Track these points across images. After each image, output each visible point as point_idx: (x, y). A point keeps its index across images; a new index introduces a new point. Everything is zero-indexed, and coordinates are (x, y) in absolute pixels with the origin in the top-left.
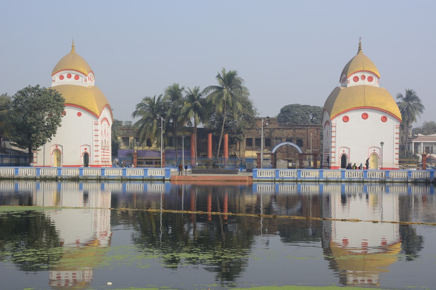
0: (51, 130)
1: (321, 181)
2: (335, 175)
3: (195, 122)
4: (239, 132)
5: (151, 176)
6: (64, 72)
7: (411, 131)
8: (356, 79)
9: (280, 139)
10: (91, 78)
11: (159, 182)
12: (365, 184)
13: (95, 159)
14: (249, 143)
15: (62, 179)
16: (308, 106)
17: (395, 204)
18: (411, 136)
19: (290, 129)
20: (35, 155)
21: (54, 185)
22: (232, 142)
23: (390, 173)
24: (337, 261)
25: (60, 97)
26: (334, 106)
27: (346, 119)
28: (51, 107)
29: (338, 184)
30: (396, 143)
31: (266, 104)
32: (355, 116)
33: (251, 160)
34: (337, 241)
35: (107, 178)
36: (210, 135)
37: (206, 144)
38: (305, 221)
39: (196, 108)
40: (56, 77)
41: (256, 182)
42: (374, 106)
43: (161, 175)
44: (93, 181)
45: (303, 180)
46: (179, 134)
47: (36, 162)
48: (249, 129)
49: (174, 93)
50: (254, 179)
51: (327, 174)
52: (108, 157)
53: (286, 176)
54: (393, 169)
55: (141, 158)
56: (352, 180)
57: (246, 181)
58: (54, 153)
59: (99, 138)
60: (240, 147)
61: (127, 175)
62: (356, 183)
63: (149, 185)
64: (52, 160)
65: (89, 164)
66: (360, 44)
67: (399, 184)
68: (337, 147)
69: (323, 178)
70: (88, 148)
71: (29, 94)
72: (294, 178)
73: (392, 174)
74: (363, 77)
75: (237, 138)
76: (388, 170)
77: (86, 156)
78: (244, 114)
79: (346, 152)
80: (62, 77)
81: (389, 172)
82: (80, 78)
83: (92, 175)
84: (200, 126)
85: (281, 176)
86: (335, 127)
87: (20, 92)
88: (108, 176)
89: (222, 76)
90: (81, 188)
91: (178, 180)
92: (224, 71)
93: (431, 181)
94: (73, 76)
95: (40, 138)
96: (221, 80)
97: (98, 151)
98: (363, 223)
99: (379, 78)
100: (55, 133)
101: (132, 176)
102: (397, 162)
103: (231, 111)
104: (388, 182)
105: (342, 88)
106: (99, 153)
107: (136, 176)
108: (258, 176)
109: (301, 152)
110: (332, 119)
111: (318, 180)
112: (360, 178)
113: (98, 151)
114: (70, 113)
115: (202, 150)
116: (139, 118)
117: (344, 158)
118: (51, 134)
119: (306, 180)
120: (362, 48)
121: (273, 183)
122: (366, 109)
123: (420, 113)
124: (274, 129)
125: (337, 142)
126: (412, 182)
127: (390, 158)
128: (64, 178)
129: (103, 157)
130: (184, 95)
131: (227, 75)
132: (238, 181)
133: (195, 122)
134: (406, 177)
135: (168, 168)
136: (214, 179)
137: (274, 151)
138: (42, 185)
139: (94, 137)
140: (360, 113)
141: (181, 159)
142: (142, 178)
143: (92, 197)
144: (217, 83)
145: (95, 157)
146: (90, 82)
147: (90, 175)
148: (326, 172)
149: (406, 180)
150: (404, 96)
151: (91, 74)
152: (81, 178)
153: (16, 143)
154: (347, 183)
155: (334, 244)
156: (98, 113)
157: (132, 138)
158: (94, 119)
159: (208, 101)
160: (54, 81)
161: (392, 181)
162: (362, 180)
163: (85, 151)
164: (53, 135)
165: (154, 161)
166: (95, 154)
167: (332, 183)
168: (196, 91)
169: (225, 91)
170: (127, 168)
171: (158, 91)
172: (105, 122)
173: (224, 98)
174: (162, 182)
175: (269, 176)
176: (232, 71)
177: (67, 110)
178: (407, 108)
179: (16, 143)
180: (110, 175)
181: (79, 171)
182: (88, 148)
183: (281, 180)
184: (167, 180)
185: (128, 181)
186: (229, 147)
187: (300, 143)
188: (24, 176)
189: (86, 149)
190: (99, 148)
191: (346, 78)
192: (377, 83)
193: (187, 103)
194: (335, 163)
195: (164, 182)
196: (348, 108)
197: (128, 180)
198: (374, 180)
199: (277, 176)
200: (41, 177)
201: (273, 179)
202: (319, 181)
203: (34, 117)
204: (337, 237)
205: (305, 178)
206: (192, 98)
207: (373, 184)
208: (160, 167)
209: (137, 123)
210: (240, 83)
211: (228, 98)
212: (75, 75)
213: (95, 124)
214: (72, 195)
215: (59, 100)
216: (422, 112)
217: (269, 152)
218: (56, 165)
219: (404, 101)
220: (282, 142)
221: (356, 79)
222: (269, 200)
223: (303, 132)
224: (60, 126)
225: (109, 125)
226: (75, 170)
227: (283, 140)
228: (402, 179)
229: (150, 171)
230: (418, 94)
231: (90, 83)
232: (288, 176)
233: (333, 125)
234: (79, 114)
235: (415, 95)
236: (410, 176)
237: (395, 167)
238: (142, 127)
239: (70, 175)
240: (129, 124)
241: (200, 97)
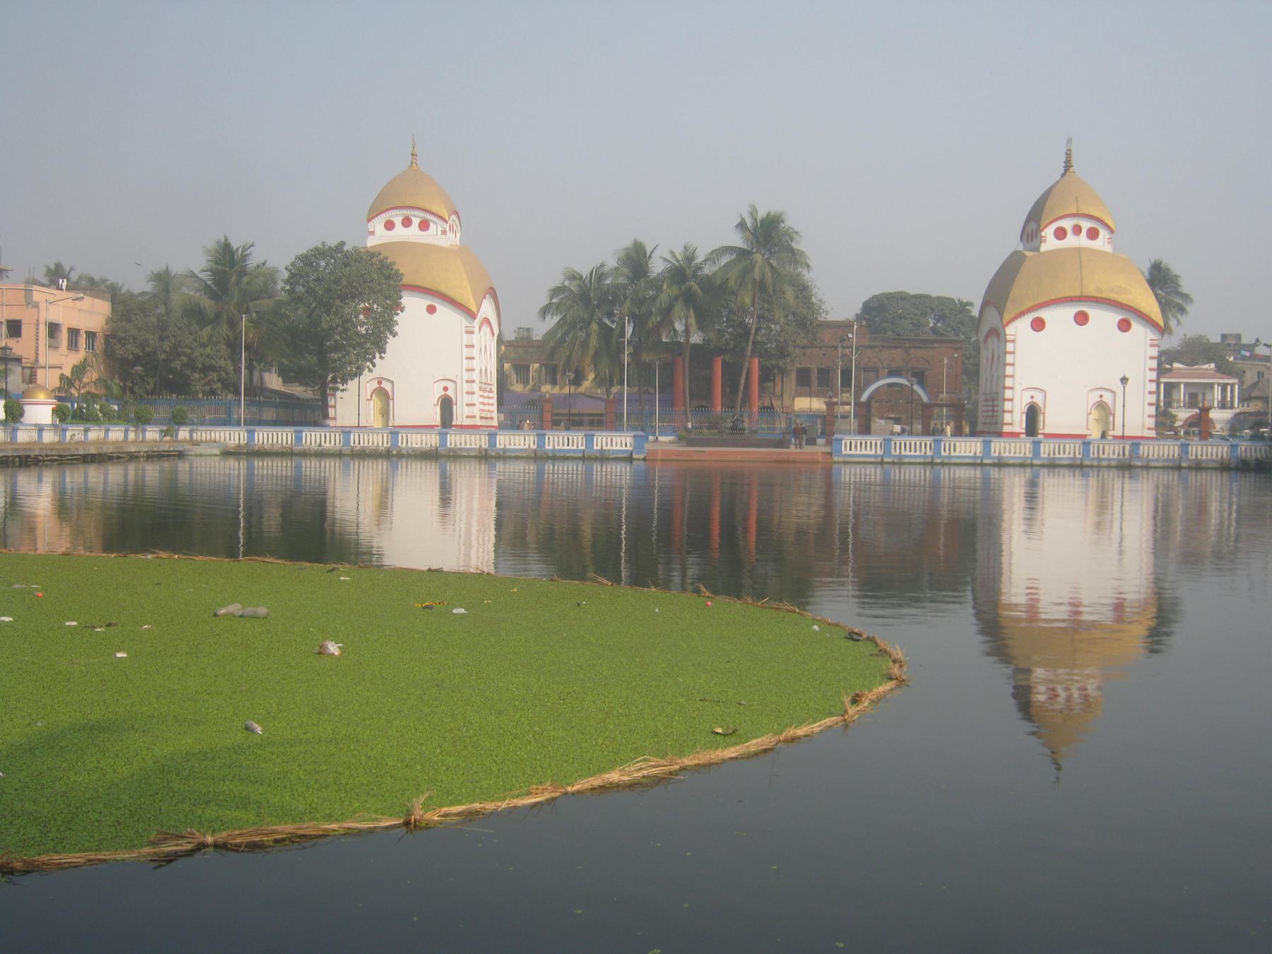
0: (376, 342)
1: (987, 465)
6: (395, 212)
8: (1061, 234)
13: (467, 411)
15: (400, 456)
16: (927, 297)
19: (896, 348)
20: (331, 402)
21: (382, 465)
22: (767, 375)
26: (1011, 296)
27: (1038, 325)
31: (839, 293)
33: (812, 416)
34: (1014, 600)
37: (709, 382)
38: (944, 552)
39: (688, 298)
40: (378, 225)
42: (1104, 296)
46: (646, 357)
47: (334, 419)
48: (804, 347)
49: (636, 259)
50: (836, 459)
51: (999, 448)
52: (491, 408)
54: (1142, 438)
64: (371, 415)
66: (1068, 154)
68: (1018, 388)
69: (990, 458)
70: (450, 385)
71: (323, 264)
72: (925, 456)
73: (1144, 450)
74: (1077, 230)
76: (1136, 442)
77: (447, 405)
78: (793, 314)
79: (1038, 400)
80: (390, 225)
82: (432, 226)
84: (696, 338)
87: (303, 258)
88: (505, 450)
89: (749, 225)
92: (753, 212)
94: (416, 221)
97: (473, 393)
100: (382, 351)
101: (560, 450)
102: (1151, 422)
103: (766, 306)
105: (1028, 254)
106: (476, 399)
107: (569, 451)
109: (925, 399)
110: (1007, 324)
112: (1075, 458)
113: (473, 393)
114: (413, 304)
115: (701, 394)
116: (552, 321)
117: (1033, 414)
119: (954, 461)
120: (1074, 162)
122: (1084, 302)
125: (1017, 376)
127: (1136, 416)
129: (482, 407)
130: (657, 267)
131: (762, 221)
133: (685, 328)
135: (888, 437)
137: (864, 398)
138: (354, 465)
140: (1070, 311)
151: (454, 217)
155: (1011, 607)
156: (474, 308)
157: (536, 366)
159: (718, 282)
160: (373, 233)
164: (377, 355)
166: (467, 399)
169: (758, 257)
171: (598, 253)
172: (486, 328)
173: (757, 273)
175: (868, 452)
177: (408, 300)
182: (450, 385)
186: (762, 389)
187: (920, 377)
188: (314, 447)
189: (446, 389)
190: (475, 387)
191: (1039, 230)
193: (669, 286)
196: (1041, 300)
197: (548, 458)
198: (1105, 463)
199: (887, 451)
204: (1014, 591)
205: (950, 457)
206: (681, 273)
209: (550, 334)
210: (792, 239)
213: (467, 332)
214: (1065, 500)
215: (388, 277)
218: (378, 424)
220: (877, 379)
221: (1061, 234)
223: (937, 357)
224: (395, 335)
228: (1168, 460)
231: (452, 240)
232: (912, 453)
233: (1008, 338)
234: (431, 309)
236: (1187, 453)
238: (563, 340)
240: (525, 334)
241: (699, 273)
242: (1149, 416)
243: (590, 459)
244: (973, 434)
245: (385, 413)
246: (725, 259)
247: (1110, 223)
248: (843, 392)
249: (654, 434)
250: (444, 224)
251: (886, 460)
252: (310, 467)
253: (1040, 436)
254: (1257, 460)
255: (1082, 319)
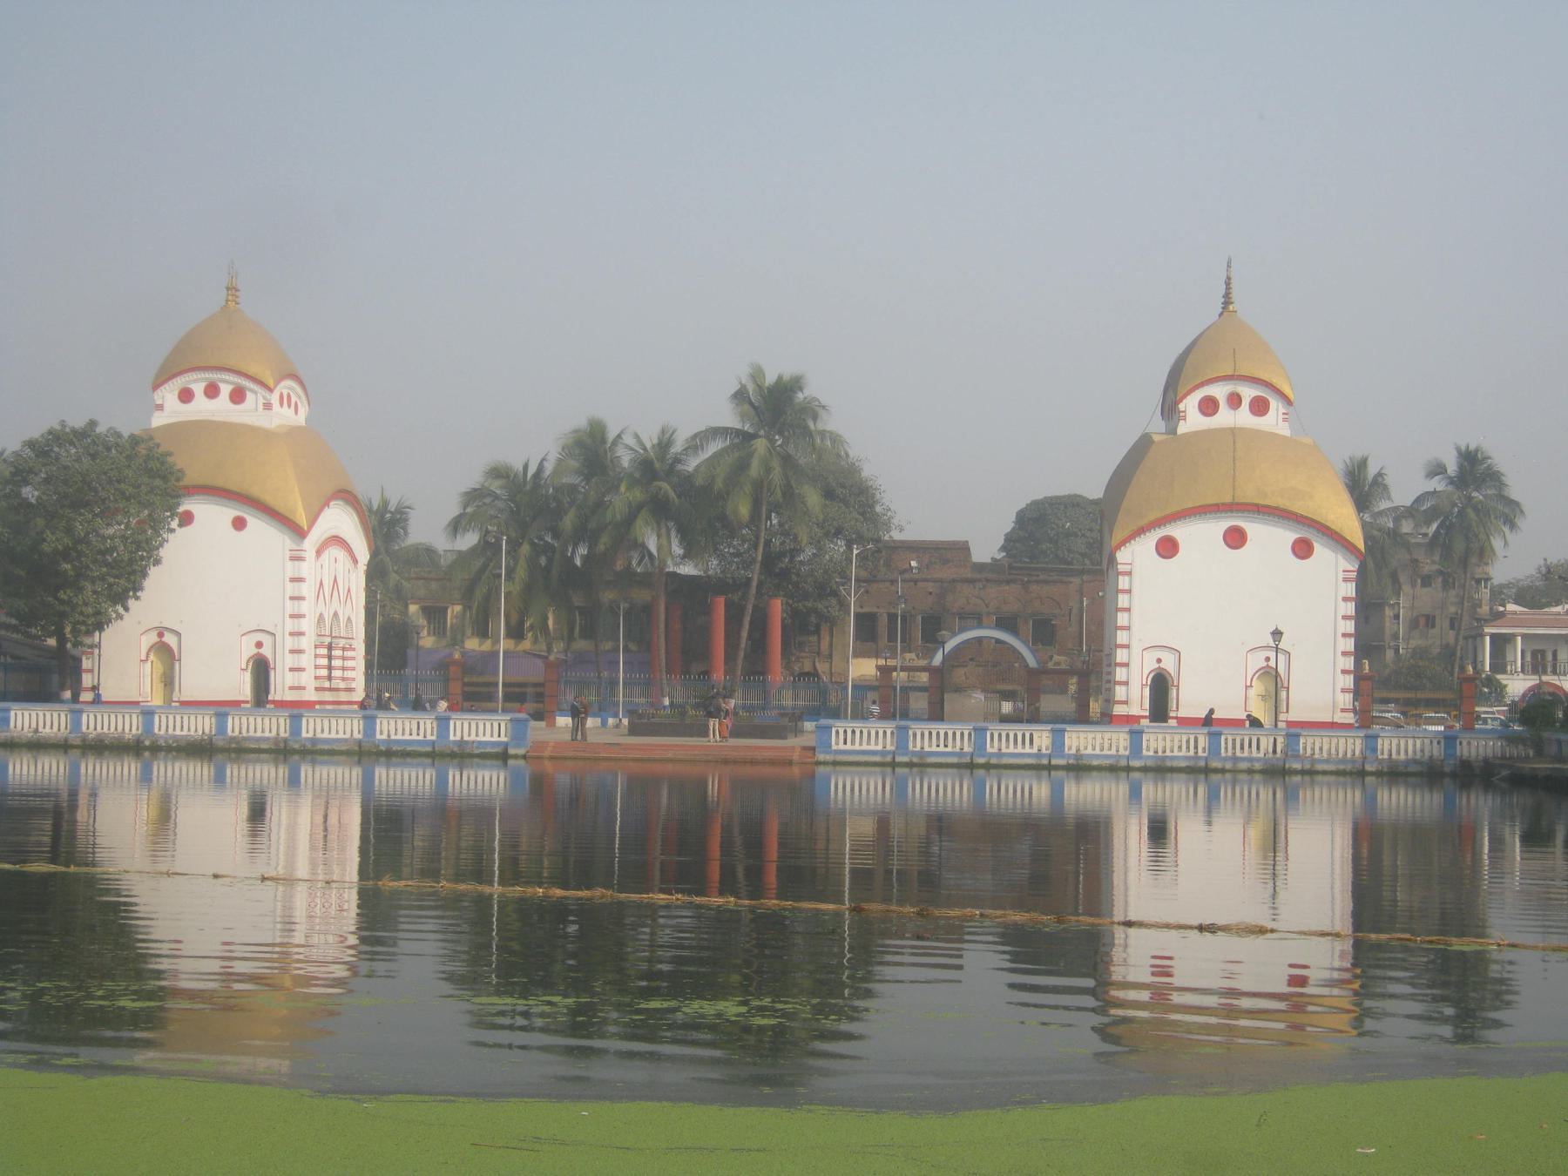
0: (125, 576)
1: (1057, 768)
2: (1106, 745)
3: (665, 550)
4: (825, 590)
5: (462, 743)
7: (1485, 593)
8: (1208, 406)
9: (974, 618)
10: (294, 399)
11: (488, 762)
12: (1215, 778)
13: (290, 679)
14: (868, 629)
15: (156, 749)
17: (1337, 854)
18: (1485, 609)
19: (1008, 582)
23: (1302, 740)
24: (1142, 1049)
25: (162, 463)
26: (1125, 504)
27: (1168, 548)
28: (128, 499)
29: (1118, 779)
30: (1344, 635)
32: (1200, 537)
35: (309, 746)
36: (720, 603)
40: (168, 395)
41: (829, 769)
43: (495, 738)
44: (263, 756)
45: (994, 761)
49: (591, 449)
50: (821, 757)
53: (934, 749)
55: (475, 679)
56: (1169, 764)
57: (790, 763)
58: (152, 657)
59: (305, 607)
60: (831, 645)
61: (378, 736)
62: (1183, 776)
63: (453, 775)
65: (270, 698)
67: (1332, 778)
68: (1136, 648)
69: (1063, 756)
72: (961, 754)
74: (1235, 401)
75: (815, 611)
76: (221, 709)
77: (261, 670)
79: (1169, 664)
80: (186, 396)
81: (1298, 736)
82: (250, 396)
83: (259, 734)
84: (687, 569)
85: (915, 745)
86: (1129, 574)
87: (31, 444)
88: (314, 741)
90: (146, 778)
91: (552, 758)
93: (1447, 769)
94: (226, 390)
95: (86, 604)
96: (747, 407)
98: (1229, 906)
99: (1289, 402)
101: (398, 742)
102: (1346, 700)
104: (1296, 772)
108: (834, 747)
109: (1032, 662)
110: (1119, 547)
111: (1045, 762)
112: (1196, 757)
115: (690, 655)
117: (1161, 686)
118: (127, 590)
119: (1005, 761)
120: (1235, 296)
121: (889, 770)
122: (1238, 511)
123: (1506, 529)
124: (954, 581)
126: (1378, 774)
127: (1322, 684)
128: (162, 742)
132: (764, 762)
133: (665, 550)
134: (1357, 753)
135: (981, 724)
136: (768, 754)
139: (289, 603)
140: (1216, 528)
141: (613, 683)
142: (429, 749)
143: (279, 812)
144: (728, 417)
145: (289, 675)
146: (287, 412)
147: (252, 733)
148: (1074, 735)
149: (1358, 766)
150: (1452, 468)
152: (221, 744)
153: (14, 621)
154: (1150, 775)
156: (304, 525)
157: (458, 608)
158: (1340, 558)
160: (160, 407)
161: (1308, 766)
162: (1202, 764)
163: (255, 651)
165: (530, 690)
166: (290, 660)
167: (1094, 774)
168: (664, 444)
170: (380, 714)
171: (536, 445)
172: (335, 552)
173: (755, 469)
174: (499, 763)
175: (872, 747)
176: (786, 377)
178: (1462, 513)
179: (14, 621)
180: (319, 735)
181: (1127, 736)
183: (915, 760)
184: (516, 757)
185: (383, 759)
187: (1044, 633)
188: (27, 733)
189: (259, 645)
192: (1285, 420)
193: (628, 489)
194: (1126, 703)
195: (506, 764)
196: (1174, 509)
198: (1243, 766)
200: (84, 740)
201: (889, 759)
202: (1050, 768)
203: (69, 530)
205: (1000, 754)
207: (1243, 777)
208: (495, 711)
211: (768, 470)
212: (230, 387)
213: (293, 559)
214: (210, 818)
216: (1513, 526)
217: (923, 663)
219: (1450, 488)
220: (980, 626)
221: (1208, 406)
222: (923, 832)
225: (355, 561)
226: (200, 718)
227: (985, 620)
228: (1344, 760)
229: (459, 724)
230: (1502, 458)
232: (942, 748)
234: (239, 524)
235: (1489, 467)
236: (1375, 750)
237: (1341, 718)
239: (185, 732)
241: (679, 467)
242: (1344, 691)
243: (442, 755)
244: (884, 716)
245: (168, 681)
246: (713, 448)
247: (1287, 390)
248: (903, 650)
249: (616, 715)
250: (267, 394)
251: (898, 759)
252: (91, 769)
253: (1172, 722)
254: (1486, 760)
255: (1236, 538)
